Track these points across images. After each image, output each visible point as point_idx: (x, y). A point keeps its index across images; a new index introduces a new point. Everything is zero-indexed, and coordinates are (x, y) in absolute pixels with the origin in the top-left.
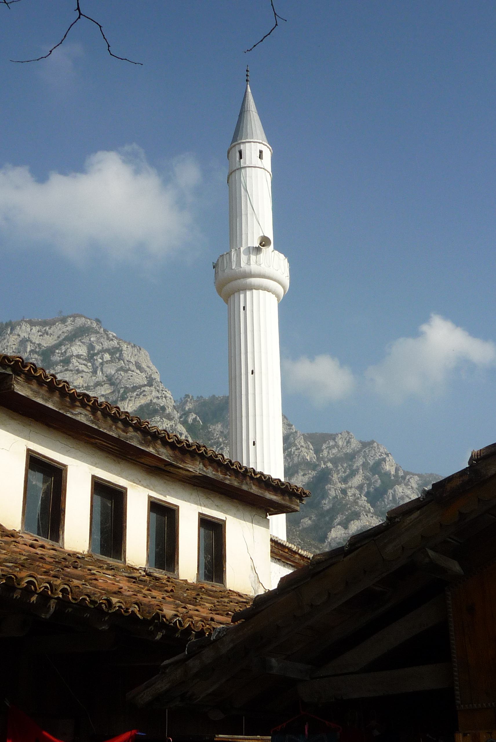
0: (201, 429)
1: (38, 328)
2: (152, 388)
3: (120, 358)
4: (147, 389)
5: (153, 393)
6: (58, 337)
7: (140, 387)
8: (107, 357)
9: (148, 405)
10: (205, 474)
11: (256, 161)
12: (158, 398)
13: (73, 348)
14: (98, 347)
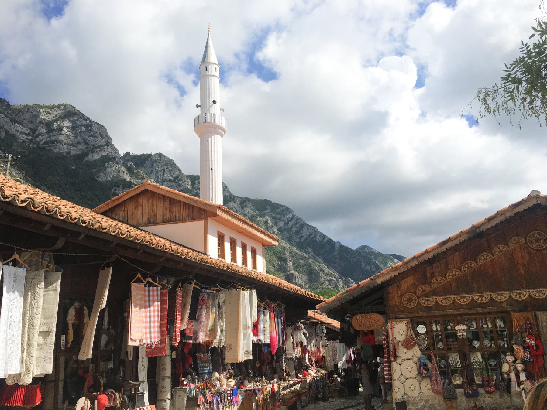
0: (482, 386)
1: (44, 110)
2: (109, 147)
3: (91, 130)
4: (105, 147)
5: (109, 150)
6: (56, 116)
7: (102, 146)
8: (84, 129)
9: (106, 156)
10: (533, 390)
11: (214, 73)
12: (111, 152)
13: (64, 123)
14: (79, 123)
